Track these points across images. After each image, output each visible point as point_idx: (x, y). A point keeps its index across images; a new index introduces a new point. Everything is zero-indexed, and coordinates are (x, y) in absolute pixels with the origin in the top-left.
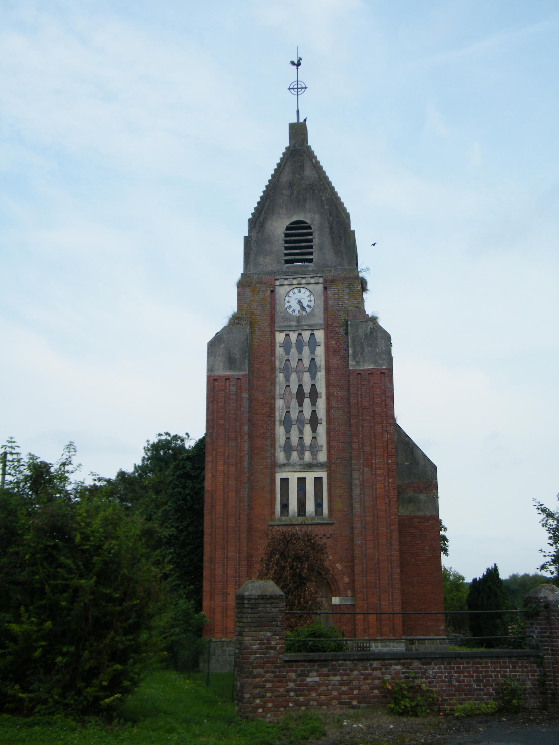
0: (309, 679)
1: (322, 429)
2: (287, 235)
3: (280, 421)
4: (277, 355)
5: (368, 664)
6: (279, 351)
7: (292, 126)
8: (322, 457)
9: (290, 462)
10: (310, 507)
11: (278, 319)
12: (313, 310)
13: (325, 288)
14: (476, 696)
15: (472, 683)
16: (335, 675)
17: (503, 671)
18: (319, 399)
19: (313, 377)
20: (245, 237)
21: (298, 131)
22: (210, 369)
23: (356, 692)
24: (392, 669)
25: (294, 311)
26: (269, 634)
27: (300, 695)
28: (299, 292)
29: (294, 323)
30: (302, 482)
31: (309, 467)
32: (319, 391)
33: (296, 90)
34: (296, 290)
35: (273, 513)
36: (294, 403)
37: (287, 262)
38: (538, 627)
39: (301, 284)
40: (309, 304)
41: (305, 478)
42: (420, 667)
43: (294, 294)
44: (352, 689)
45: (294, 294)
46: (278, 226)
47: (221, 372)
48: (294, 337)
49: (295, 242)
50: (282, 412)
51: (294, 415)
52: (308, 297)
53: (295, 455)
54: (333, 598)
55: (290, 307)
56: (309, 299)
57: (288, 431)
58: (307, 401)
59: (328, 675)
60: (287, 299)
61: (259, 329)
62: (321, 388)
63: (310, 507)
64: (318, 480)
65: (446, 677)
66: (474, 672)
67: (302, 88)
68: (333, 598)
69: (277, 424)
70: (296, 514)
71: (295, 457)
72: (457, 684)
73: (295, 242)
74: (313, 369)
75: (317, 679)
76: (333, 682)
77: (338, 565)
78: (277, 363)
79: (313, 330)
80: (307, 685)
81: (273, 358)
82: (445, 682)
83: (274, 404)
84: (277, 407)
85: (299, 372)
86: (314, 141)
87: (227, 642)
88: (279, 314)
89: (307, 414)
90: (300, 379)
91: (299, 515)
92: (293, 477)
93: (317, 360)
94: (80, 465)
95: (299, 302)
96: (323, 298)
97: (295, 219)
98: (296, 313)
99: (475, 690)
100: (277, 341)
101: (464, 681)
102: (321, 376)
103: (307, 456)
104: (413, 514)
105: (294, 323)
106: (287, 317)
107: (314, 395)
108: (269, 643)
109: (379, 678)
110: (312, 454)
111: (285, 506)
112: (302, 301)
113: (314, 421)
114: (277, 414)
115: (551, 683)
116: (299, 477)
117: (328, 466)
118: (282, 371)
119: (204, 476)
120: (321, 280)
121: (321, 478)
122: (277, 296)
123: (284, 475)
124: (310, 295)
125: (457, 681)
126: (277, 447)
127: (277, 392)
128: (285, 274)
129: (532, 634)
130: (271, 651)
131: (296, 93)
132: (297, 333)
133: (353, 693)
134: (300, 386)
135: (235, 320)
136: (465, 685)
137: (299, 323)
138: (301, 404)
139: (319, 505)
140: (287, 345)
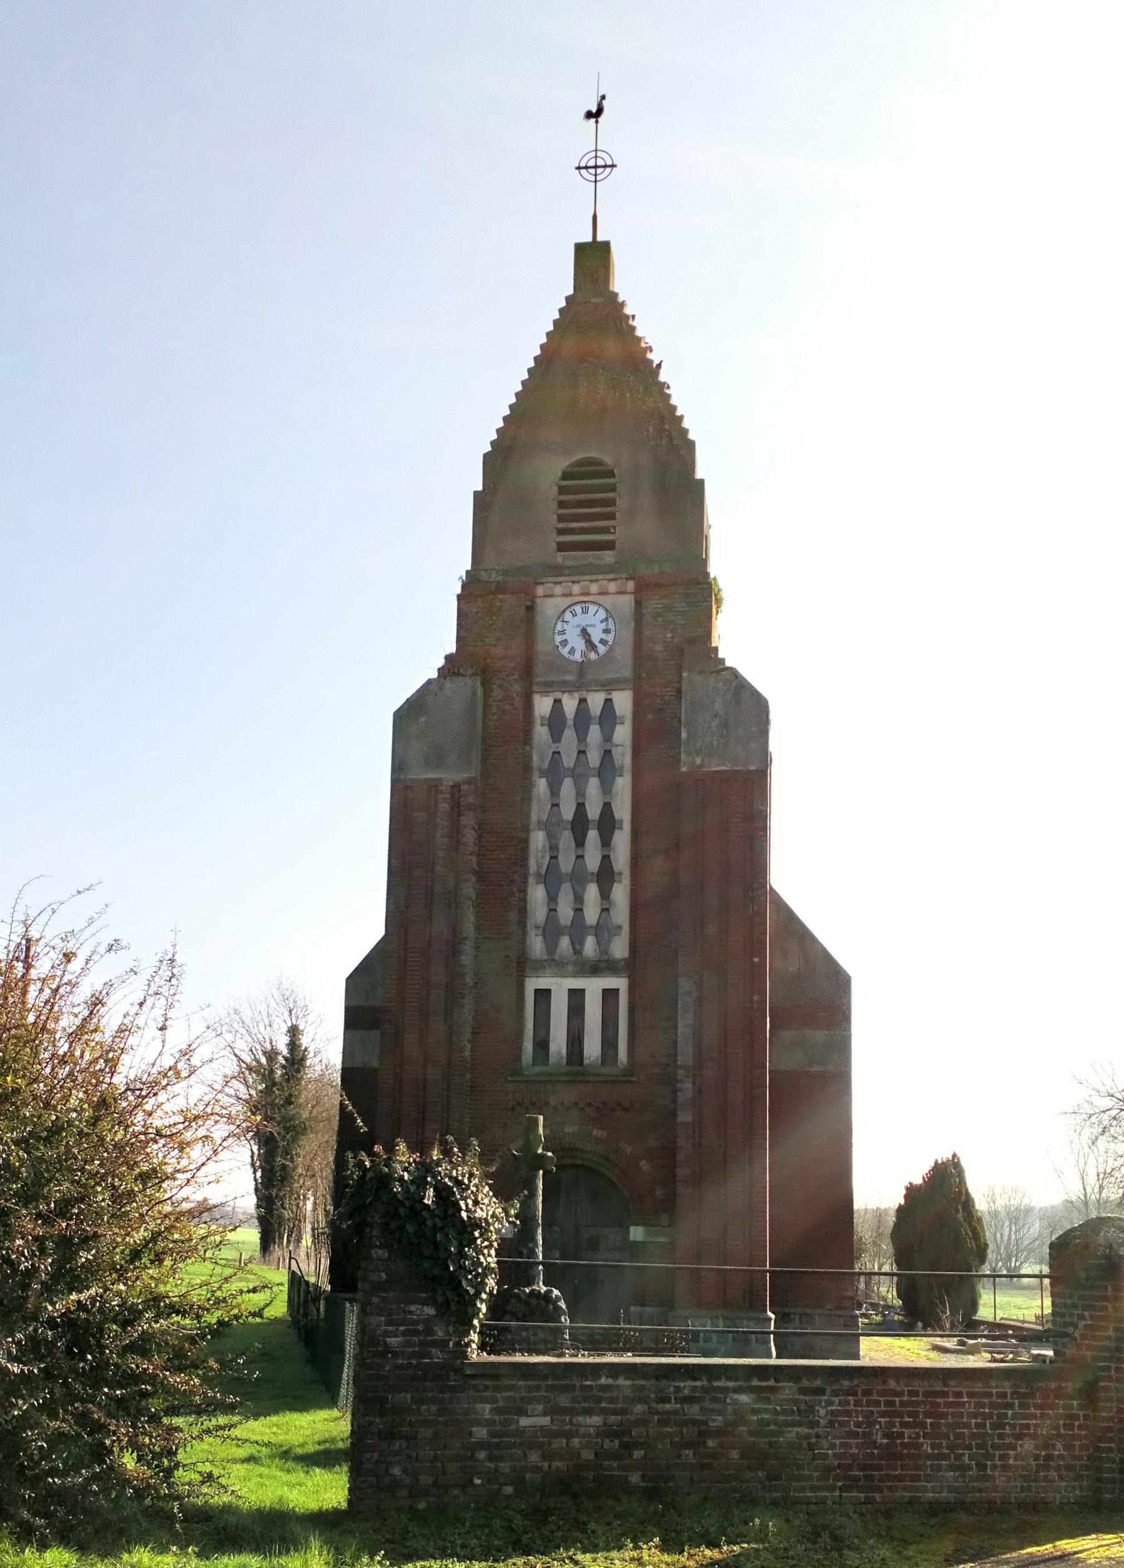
0: (524, 1422)
1: (620, 893)
2: (562, 490)
3: (538, 874)
4: (536, 740)
5: (672, 1389)
6: (541, 733)
7: (580, 248)
8: (620, 949)
9: (556, 957)
10: (592, 1048)
11: (539, 669)
12: (611, 650)
13: (638, 603)
14: (929, 1471)
15: (922, 1440)
16: (588, 1412)
17: (998, 1415)
18: (617, 832)
19: (607, 787)
20: (475, 492)
21: (593, 258)
22: (398, 766)
23: (638, 1454)
24: (728, 1401)
25: (572, 651)
26: (430, 1311)
27: (501, 1459)
28: (585, 611)
30: (576, 997)
31: (595, 969)
32: (617, 816)
33: (592, 171)
35: (518, 1057)
36: (566, 838)
37: (562, 547)
38: (1086, 1313)
39: (588, 594)
40: (604, 636)
41: (584, 990)
42: (797, 1400)
43: (574, 615)
44: (627, 1447)
45: (574, 615)
46: (547, 471)
47: (418, 774)
48: (570, 705)
49: (580, 504)
50: (543, 857)
51: (566, 863)
52: (601, 622)
53: (565, 942)
54: (632, 1229)
55: (565, 643)
56: (603, 626)
57: (552, 898)
58: (593, 835)
59: (572, 1412)
60: (559, 627)
61: (500, 687)
63: (592, 1048)
64: (609, 995)
65: (858, 1425)
66: (927, 1415)
67: (605, 166)
68: (632, 1229)
69: (531, 880)
70: (565, 1062)
72: (885, 1441)
73: (580, 504)
74: (607, 770)
75: (546, 1421)
76: (582, 1430)
77: (642, 1163)
78: (535, 758)
79: (609, 691)
80: (520, 1432)
81: (527, 748)
82: (855, 1435)
83: (526, 841)
84: (532, 847)
85: (579, 778)
86: (624, 282)
89: (593, 862)
90: (580, 793)
92: (560, 986)
93: (616, 752)
95: (585, 633)
96: (633, 624)
97: (580, 456)
98: (577, 657)
99: (930, 1457)
100: (537, 713)
101: (901, 1435)
102: (623, 785)
103: (590, 946)
105: (570, 677)
106: (559, 663)
107: (607, 824)
108: (429, 1331)
109: (694, 1422)
110: (598, 943)
111: (542, 1044)
112: (589, 630)
113: (606, 876)
114: (532, 862)
115: (1113, 1445)
117: (631, 967)
118: (543, 773)
120: (631, 585)
122: (539, 619)
123: (542, 983)
124: (606, 619)
125: (885, 1436)
126: (528, 928)
127: (534, 817)
128: (557, 571)
129: (1071, 1330)
130: (434, 1350)
131: (593, 178)
132: (577, 696)
133: (631, 1456)
134: (581, 807)
135: (451, 667)
136: (905, 1446)
137: (582, 677)
138: (580, 843)
139: (609, 1043)
140: (556, 720)
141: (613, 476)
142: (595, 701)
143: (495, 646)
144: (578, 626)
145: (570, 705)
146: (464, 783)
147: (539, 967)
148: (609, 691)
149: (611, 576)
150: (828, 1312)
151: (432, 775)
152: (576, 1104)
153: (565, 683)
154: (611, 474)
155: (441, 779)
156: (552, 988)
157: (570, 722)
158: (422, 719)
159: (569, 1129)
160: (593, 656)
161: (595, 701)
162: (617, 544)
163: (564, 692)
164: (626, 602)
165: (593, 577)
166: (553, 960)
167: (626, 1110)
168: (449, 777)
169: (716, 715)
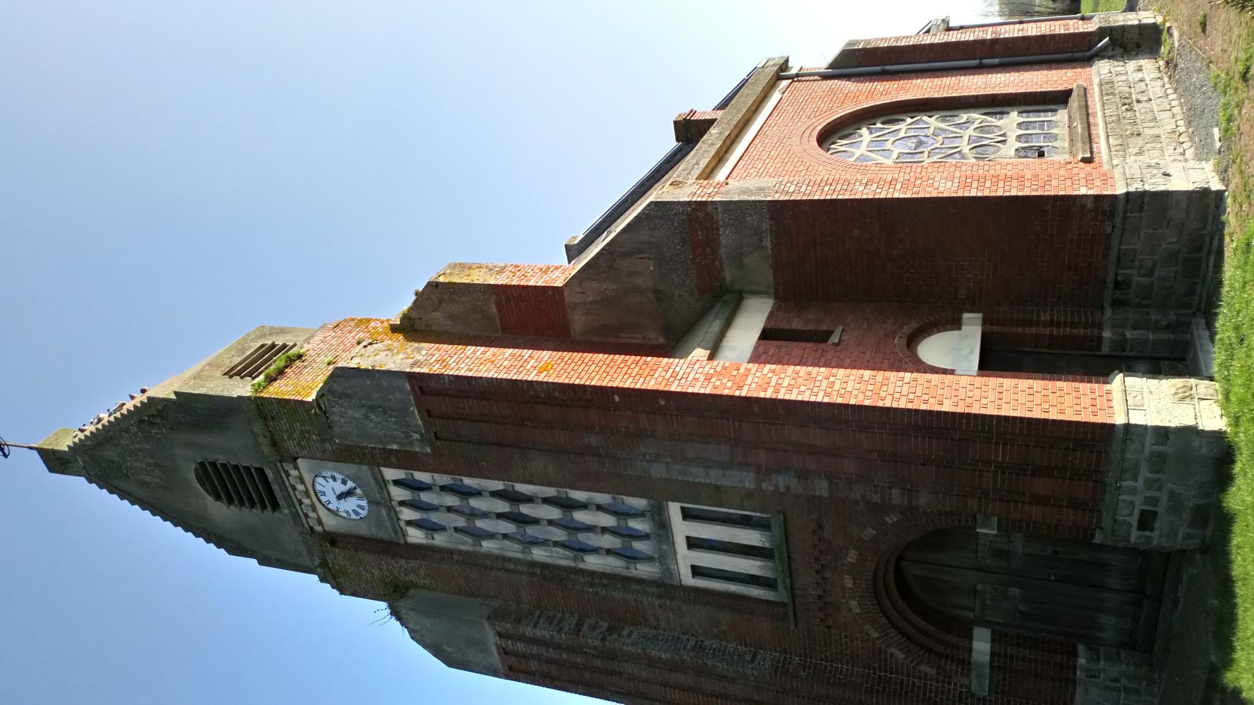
10: (751, 537)
21: (56, 461)
31: (663, 527)
35: (768, 602)
48: (407, 514)
63: (751, 537)
69: (582, 566)
88: (374, 531)
94: (1168, 175)
95: (341, 497)
104: (768, 242)
114: (563, 563)
116: (685, 546)
119: (668, 263)
132: (398, 509)
146: (494, 628)
147: (668, 572)
150: (1117, 233)
152: (817, 571)
157: (425, 516)
161: (398, 494)
163: (398, 519)
168: (492, 639)
169: (366, 417)
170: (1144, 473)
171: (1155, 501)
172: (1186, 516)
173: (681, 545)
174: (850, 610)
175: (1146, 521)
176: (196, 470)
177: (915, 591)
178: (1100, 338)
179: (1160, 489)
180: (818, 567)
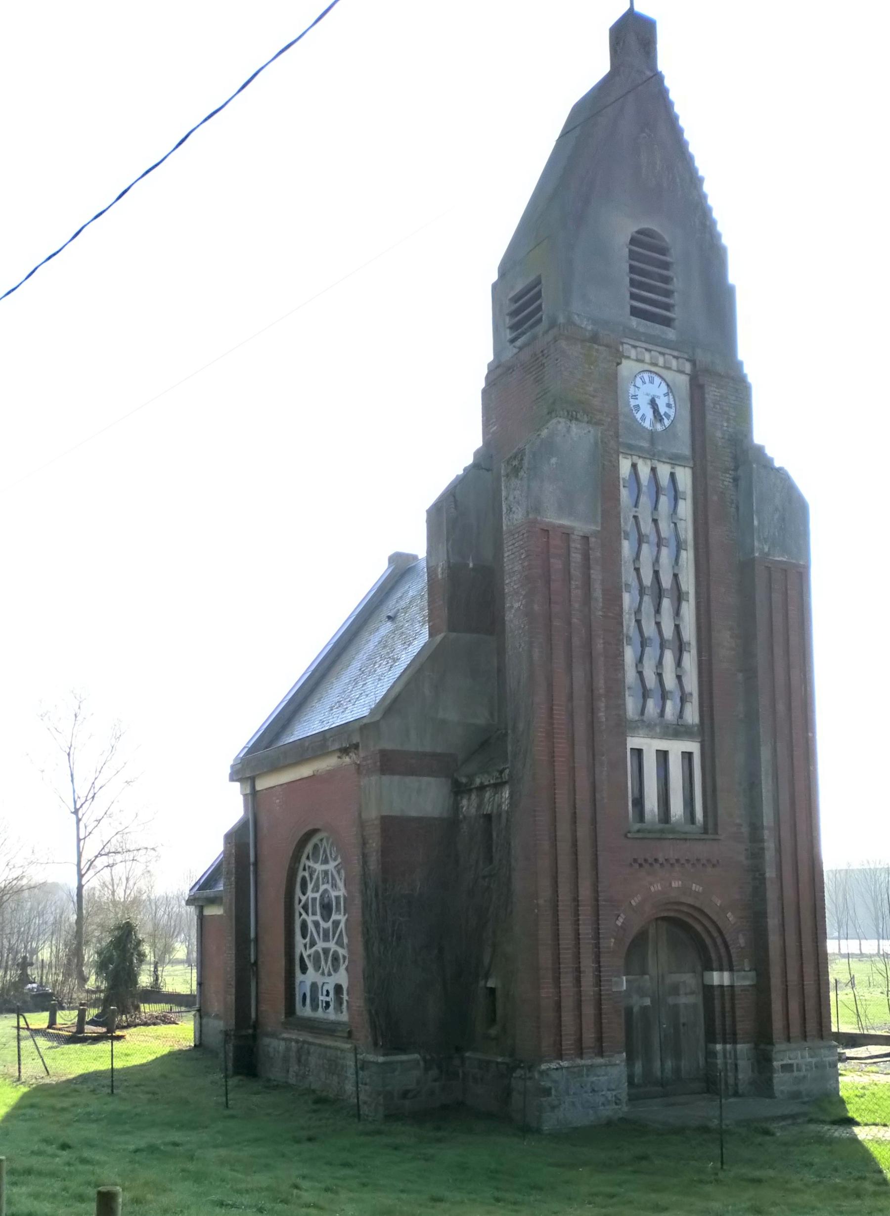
8: (692, 715)
29: (645, 444)
30: (663, 756)
31: (678, 731)
34: (646, 376)
58: (666, 603)
62: (688, 584)
64: (688, 756)
71: (651, 711)
86: (670, 60)
87: (587, 1066)
91: (660, 821)
92: (650, 746)
95: (653, 403)
103: (671, 709)
105: (645, 444)
111: (639, 802)
121: (313, 891)
141: (630, 251)
142: (664, 471)
143: (594, 396)
144: (647, 394)
145: (644, 471)
148: (673, 465)
149: (676, 353)
151: (565, 522)
153: (641, 449)
154: (663, 251)
155: (573, 528)
156: (644, 748)
158: (553, 460)
159: (675, 884)
160: (659, 427)
162: (677, 323)
164: (682, 381)
165: (650, 347)
166: (643, 721)
167: (714, 866)
170: (814, 1060)
171: (799, 1070)
172: (795, 1088)
173: (663, 745)
174: (651, 884)
175: (787, 1068)
176: (661, 239)
177: (687, 933)
178: (715, 1042)
179: (806, 1070)
180: (683, 861)
